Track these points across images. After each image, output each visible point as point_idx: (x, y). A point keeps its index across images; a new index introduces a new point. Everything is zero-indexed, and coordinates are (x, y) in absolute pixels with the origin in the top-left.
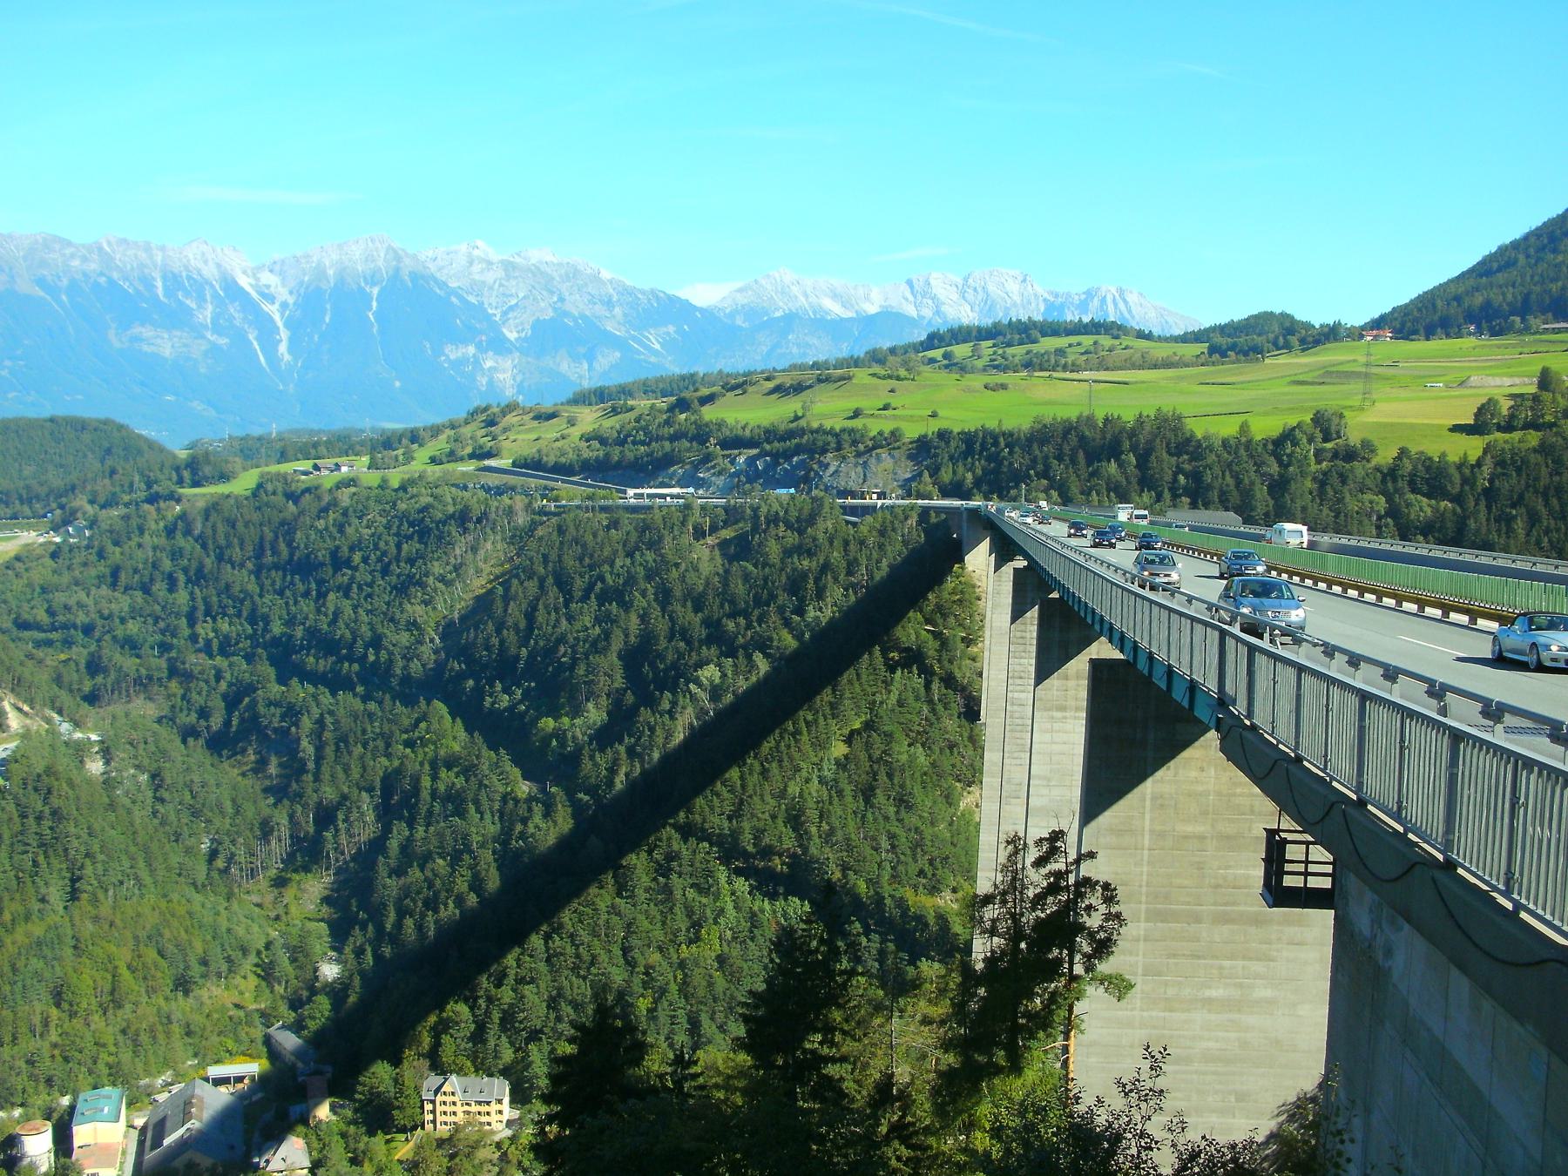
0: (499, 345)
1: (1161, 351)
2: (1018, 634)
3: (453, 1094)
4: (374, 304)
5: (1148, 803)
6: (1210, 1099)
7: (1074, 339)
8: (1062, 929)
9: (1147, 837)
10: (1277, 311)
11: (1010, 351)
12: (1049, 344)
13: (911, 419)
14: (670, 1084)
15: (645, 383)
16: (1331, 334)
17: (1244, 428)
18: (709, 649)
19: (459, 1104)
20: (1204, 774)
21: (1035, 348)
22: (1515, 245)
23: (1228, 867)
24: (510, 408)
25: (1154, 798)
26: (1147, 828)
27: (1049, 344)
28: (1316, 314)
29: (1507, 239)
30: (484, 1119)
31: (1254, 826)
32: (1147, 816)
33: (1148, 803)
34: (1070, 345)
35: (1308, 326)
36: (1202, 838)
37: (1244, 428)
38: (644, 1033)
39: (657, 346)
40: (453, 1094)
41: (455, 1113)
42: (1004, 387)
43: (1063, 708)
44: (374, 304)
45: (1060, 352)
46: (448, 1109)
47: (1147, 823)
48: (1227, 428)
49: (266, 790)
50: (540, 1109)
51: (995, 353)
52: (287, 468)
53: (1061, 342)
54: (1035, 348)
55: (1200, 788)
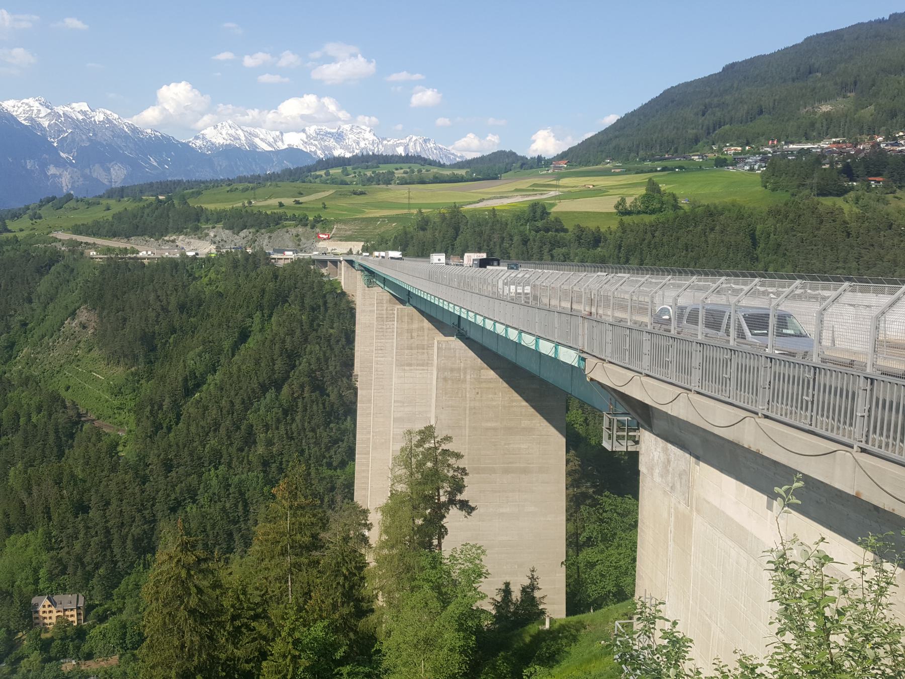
0: (62, 164)
2: (380, 327)
5: (467, 412)
6: (505, 567)
8: (433, 477)
9: (467, 429)
12: (383, 169)
15: (151, 185)
20: (496, 396)
22: (633, 113)
23: (509, 444)
24: (69, 197)
25: (470, 409)
26: (467, 425)
27: (383, 169)
29: (630, 110)
31: (523, 422)
32: (467, 419)
33: (467, 412)
38: (183, 255)
39: (155, 164)
43: (410, 365)
47: (467, 422)
50: (614, 225)
53: (391, 167)
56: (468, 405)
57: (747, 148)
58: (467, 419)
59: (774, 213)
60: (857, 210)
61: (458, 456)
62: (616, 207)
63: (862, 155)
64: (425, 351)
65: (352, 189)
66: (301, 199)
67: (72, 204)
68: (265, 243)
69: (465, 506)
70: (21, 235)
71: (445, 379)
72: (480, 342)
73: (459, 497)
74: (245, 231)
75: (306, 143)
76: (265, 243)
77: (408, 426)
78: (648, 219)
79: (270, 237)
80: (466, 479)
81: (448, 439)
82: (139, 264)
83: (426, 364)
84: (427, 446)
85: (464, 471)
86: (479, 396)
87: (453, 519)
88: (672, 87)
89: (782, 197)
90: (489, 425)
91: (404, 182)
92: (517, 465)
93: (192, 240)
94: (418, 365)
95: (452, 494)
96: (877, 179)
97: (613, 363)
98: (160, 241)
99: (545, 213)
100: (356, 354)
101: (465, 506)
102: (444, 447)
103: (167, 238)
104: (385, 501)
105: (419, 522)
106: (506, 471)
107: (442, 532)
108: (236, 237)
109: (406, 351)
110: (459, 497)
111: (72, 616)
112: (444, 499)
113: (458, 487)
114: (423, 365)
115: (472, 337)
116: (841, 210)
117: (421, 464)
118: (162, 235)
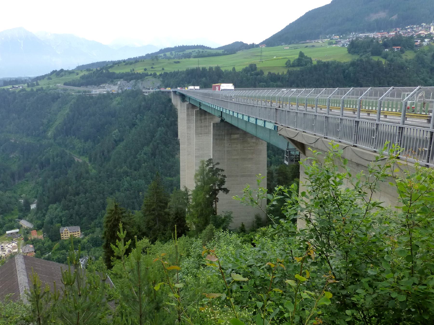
1: (214, 52)
3: (67, 231)
4: (22, 45)
5: (226, 152)
7: (193, 50)
10: (239, 41)
11: (179, 53)
12: (188, 51)
13: (158, 71)
14: (288, 281)
16: (253, 46)
17: (234, 69)
18: (424, 41)
19: (69, 233)
21: (185, 52)
23: (243, 165)
25: (227, 151)
28: (249, 42)
30: (75, 236)
32: (226, 155)
33: (226, 152)
34: (193, 51)
35: (247, 45)
36: (237, 159)
37: (234, 69)
40: (67, 231)
41: (67, 235)
42: (178, 62)
43: (201, 134)
44: (22, 45)
45: (190, 53)
46: (66, 234)
48: (230, 69)
49: (304, 153)
51: (175, 54)
52: (6, 87)
53: (190, 51)
54: (185, 52)
55: (237, 148)
56: (226, 150)
57: (341, 36)
58: (226, 155)
59: (353, 64)
60: (32, 185)
61: (222, 170)
62: (286, 64)
63: (391, 37)
64: (207, 128)
65: (174, 61)
66: (154, 67)
67: (63, 73)
68: (140, 85)
69: (226, 191)
70: (45, 87)
71: (216, 139)
72: (230, 123)
73: (223, 187)
74: (132, 81)
75: (426, 298)
76: (140, 85)
77: (202, 159)
78: (298, 69)
79: (142, 83)
80: (226, 179)
81: (218, 164)
82: (91, 97)
83: (208, 133)
84: (210, 166)
85: (224, 176)
86: (230, 145)
87: (221, 195)
88: (309, 11)
89: (356, 57)
90: (235, 157)
91: (195, 57)
92: (246, 173)
93: (111, 86)
94: (204, 134)
95: (219, 185)
96: (397, 47)
97: (411, 163)
98: (99, 87)
99: (256, 68)
100: (179, 130)
101: (226, 191)
102: (217, 167)
103: (101, 86)
104: (195, 185)
105: (208, 196)
106: (243, 176)
107: (217, 200)
108: (128, 84)
109: (200, 128)
110: (223, 187)
111: (76, 234)
112: (217, 188)
113: (222, 182)
114: (206, 134)
115: (227, 121)
116: (381, 62)
117: (207, 174)
118: (99, 85)
